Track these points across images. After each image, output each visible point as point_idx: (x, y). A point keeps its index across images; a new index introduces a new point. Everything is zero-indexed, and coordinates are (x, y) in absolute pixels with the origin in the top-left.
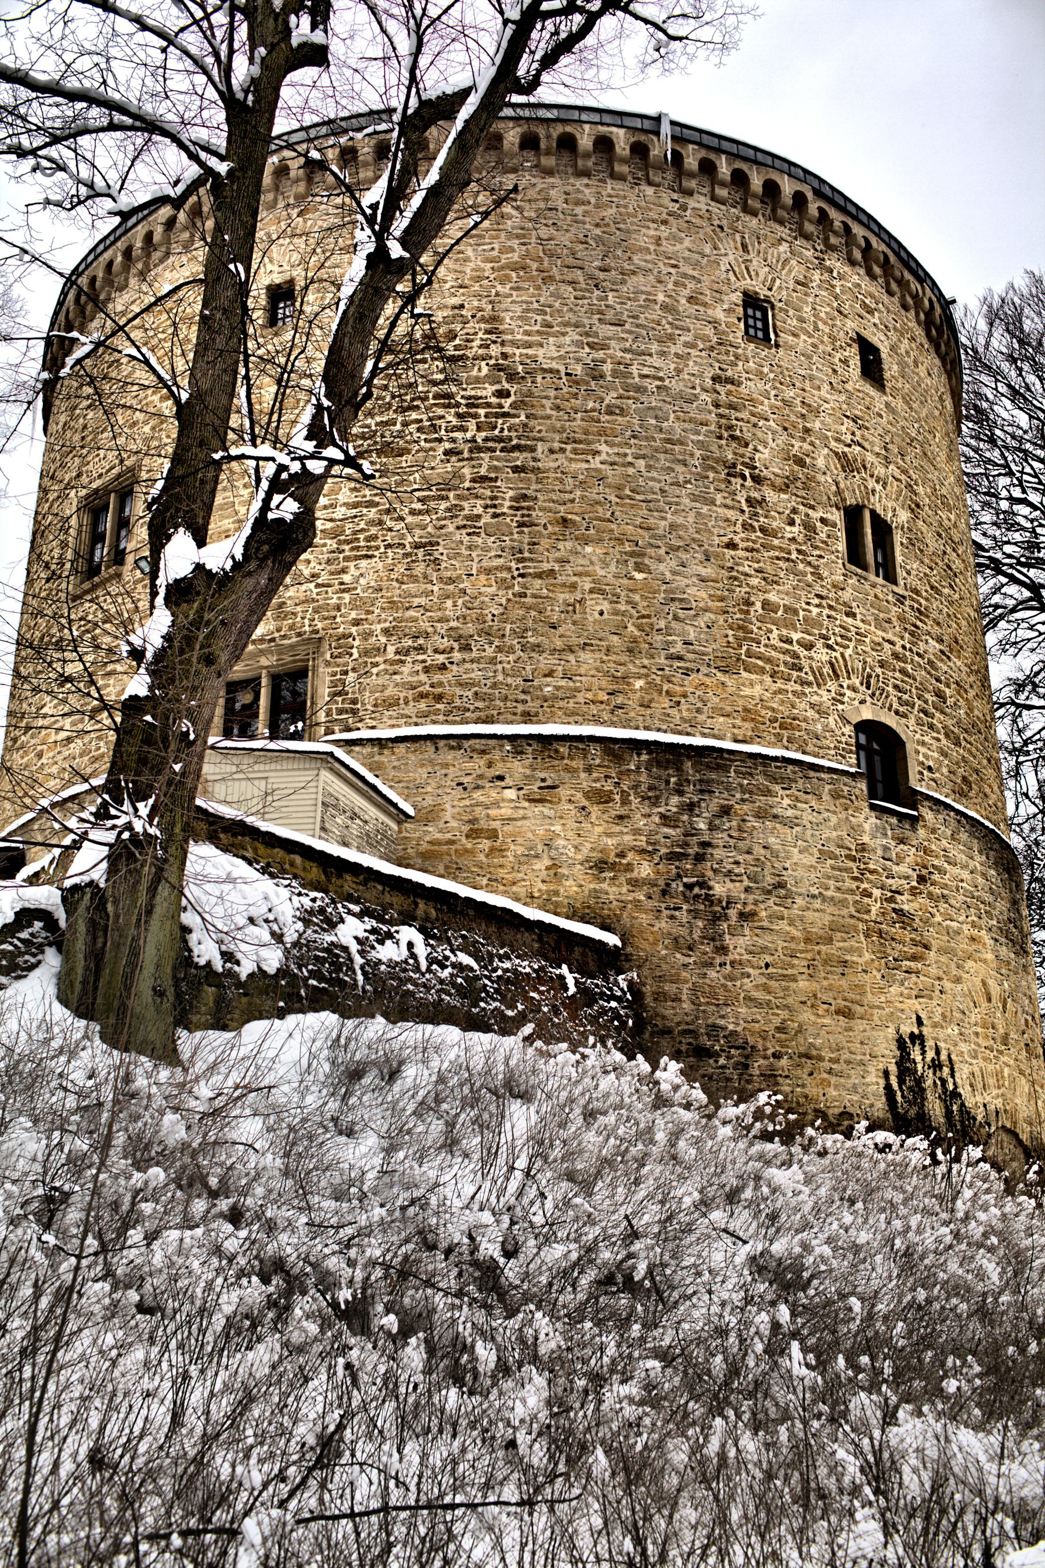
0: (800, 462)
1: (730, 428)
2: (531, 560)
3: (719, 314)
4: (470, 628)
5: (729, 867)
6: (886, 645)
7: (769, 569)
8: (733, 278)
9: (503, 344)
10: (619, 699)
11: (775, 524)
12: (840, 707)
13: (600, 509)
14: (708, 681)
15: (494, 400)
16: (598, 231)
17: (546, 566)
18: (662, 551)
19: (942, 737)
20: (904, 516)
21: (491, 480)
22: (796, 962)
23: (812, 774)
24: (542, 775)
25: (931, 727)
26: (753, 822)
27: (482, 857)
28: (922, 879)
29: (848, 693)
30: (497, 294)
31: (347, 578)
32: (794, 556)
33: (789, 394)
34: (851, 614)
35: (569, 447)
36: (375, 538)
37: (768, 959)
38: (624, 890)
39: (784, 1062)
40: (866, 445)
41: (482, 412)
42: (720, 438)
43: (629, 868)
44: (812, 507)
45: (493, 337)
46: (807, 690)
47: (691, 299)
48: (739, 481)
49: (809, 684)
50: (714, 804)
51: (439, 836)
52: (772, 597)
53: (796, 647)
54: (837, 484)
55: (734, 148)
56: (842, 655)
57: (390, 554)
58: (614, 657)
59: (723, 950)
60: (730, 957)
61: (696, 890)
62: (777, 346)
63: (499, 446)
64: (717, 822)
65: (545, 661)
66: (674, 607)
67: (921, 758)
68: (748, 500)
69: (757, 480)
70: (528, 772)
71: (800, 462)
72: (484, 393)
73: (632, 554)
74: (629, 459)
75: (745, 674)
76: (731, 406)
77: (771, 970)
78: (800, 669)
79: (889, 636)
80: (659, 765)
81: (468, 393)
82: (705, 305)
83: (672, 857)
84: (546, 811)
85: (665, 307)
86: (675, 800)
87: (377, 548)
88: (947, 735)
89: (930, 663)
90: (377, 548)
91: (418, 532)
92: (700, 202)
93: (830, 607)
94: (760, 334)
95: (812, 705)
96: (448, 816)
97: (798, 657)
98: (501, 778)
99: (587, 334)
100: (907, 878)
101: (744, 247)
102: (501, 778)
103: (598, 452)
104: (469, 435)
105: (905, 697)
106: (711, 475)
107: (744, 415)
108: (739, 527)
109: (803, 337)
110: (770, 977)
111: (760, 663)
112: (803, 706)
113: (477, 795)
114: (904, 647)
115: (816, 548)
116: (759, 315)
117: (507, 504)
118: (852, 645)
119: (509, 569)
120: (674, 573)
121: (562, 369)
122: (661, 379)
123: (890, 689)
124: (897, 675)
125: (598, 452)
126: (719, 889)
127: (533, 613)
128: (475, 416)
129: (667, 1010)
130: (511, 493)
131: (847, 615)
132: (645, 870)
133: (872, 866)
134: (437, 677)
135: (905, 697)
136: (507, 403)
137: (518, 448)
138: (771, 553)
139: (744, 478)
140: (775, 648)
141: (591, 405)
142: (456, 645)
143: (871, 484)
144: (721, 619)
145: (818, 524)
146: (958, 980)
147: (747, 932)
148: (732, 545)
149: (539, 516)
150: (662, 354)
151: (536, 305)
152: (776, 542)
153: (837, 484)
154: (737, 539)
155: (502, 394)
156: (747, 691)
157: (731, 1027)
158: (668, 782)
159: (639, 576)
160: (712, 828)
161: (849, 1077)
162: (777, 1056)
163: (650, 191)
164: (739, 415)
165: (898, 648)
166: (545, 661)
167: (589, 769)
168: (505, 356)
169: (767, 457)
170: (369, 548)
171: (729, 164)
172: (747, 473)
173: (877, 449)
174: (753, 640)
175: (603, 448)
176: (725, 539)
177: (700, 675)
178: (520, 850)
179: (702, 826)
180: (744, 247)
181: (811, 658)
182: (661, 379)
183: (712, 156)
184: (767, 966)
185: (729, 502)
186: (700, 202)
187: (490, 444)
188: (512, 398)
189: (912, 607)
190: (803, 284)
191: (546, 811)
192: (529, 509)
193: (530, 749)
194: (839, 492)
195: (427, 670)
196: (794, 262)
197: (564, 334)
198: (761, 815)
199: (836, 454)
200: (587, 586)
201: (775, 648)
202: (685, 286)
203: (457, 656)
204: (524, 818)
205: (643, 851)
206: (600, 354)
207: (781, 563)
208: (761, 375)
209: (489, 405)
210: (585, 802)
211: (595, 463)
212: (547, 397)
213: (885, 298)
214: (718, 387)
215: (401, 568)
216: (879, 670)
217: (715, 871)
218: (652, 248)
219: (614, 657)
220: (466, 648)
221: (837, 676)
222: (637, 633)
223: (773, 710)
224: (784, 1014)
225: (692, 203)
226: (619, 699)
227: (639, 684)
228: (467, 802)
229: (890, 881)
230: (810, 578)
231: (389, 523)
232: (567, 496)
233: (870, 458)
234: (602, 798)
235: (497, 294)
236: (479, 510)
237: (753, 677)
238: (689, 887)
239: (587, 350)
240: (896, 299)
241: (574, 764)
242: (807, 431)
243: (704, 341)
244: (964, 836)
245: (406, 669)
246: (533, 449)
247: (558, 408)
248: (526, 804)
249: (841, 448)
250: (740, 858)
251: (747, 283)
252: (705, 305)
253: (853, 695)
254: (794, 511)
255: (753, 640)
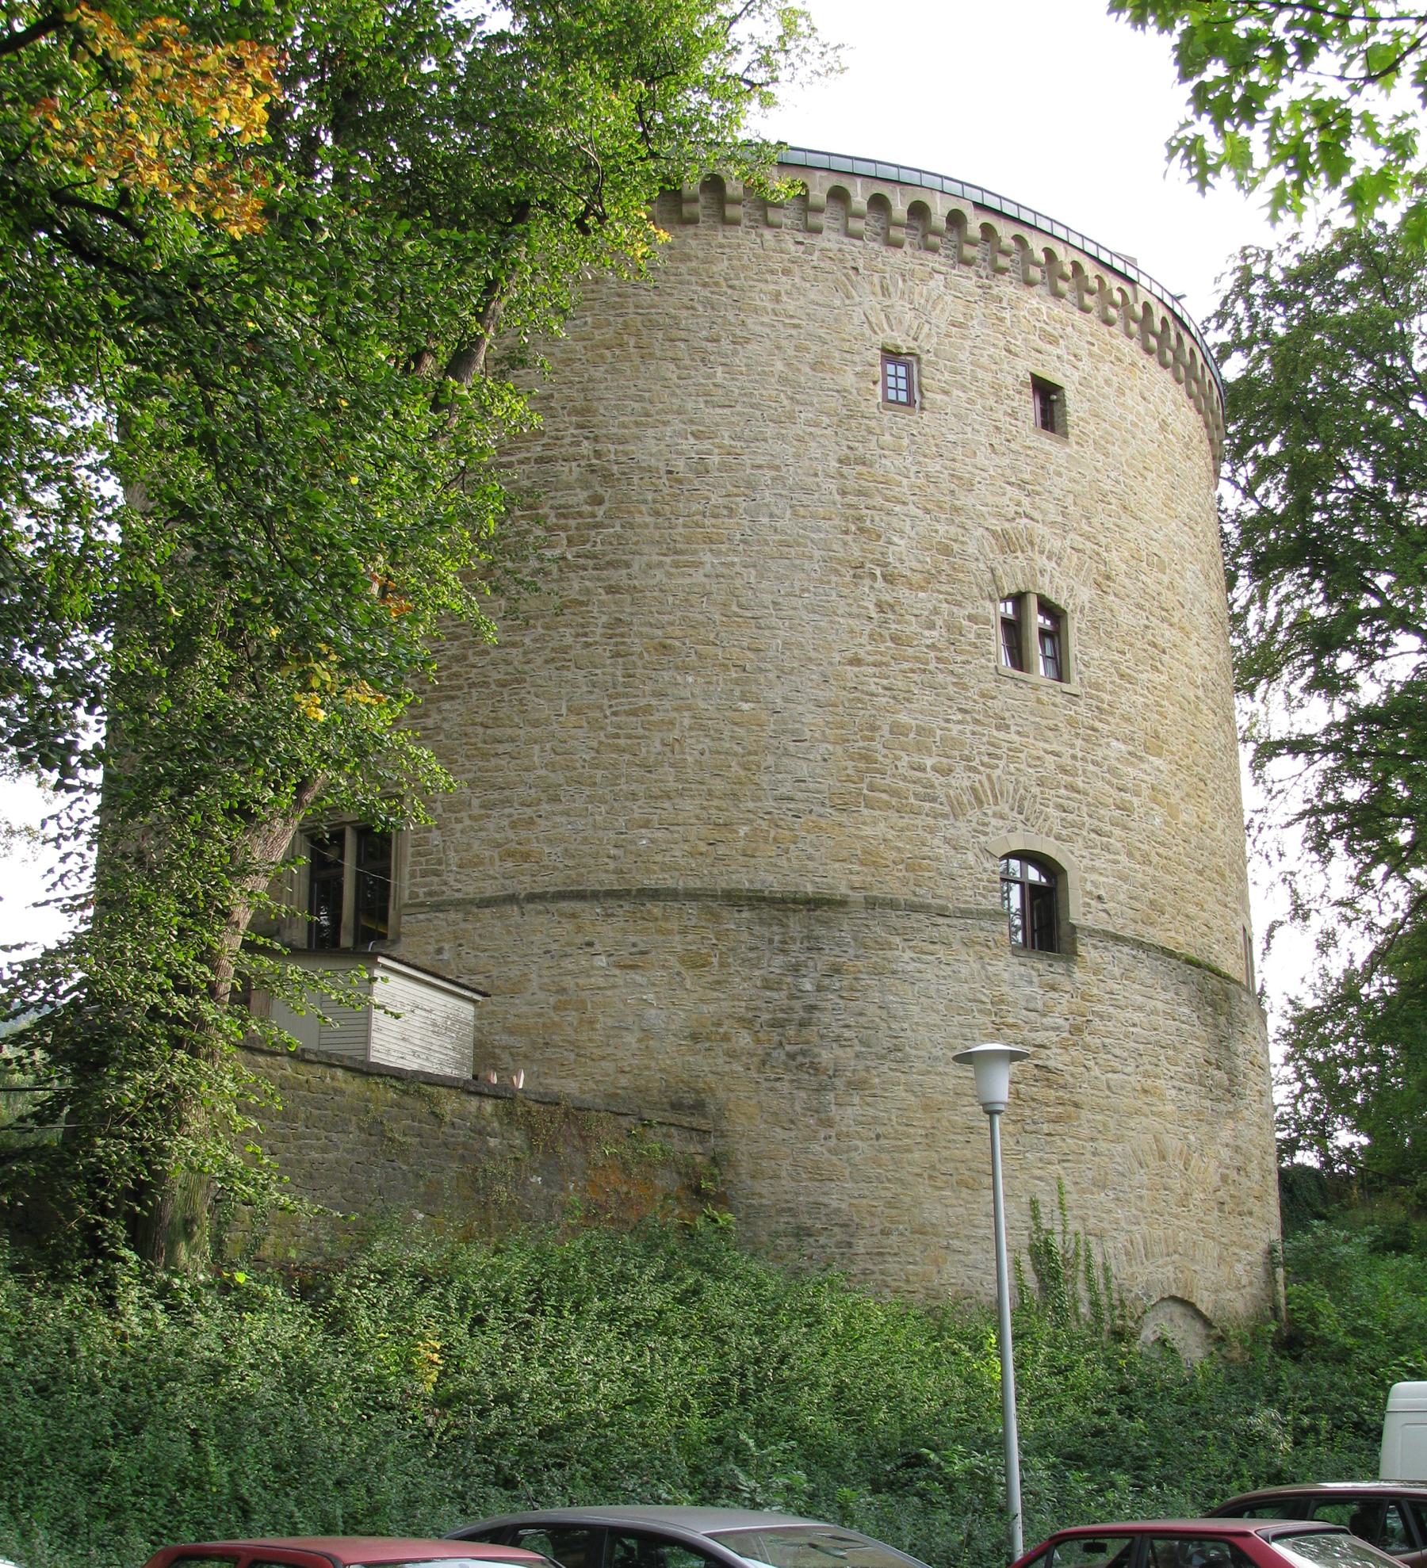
0: (946, 551)
1: (860, 519)
2: (626, 695)
3: (849, 380)
4: (559, 778)
5: (838, 1031)
6: (1050, 758)
7: (900, 684)
8: (868, 332)
9: (596, 439)
10: (721, 850)
11: (909, 630)
12: (983, 839)
13: (702, 631)
14: (823, 822)
15: (587, 508)
16: (706, 293)
17: (642, 702)
18: (772, 676)
19: (1123, 858)
20: (1085, 594)
21: (582, 603)
22: (911, 1130)
23: (940, 920)
24: (633, 939)
25: (1106, 848)
26: (867, 980)
27: (569, 1030)
28: (1076, 1030)
29: (994, 822)
30: (590, 380)
31: (429, 722)
32: (931, 667)
33: (934, 466)
34: (1003, 727)
35: (668, 560)
36: (457, 675)
37: (879, 1130)
38: (720, 1061)
39: (894, 1238)
40: (1036, 515)
41: (572, 523)
42: (846, 533)
43: (726, 1038)
44: (959, 604)
45: (585, 432)
46: (942, 822)
47: (814, 367)
48: (867, 581)
49: (945, 816)
50: (823, 962)
51: (525, 1009)
52: (903, 718)
53: (930, 774)
54: (992, 570)
55: (869, 169)
56: (989, 777)
57: (475, 694)
58: (716, 802)
59: (829, 1123)
60: (837, 1128)
61: (800, 1059)
62: (922, 409)
63: (590, 563)
64: (826, 982)
65: (637, 811)
66: (786, 740)
67: (1089, 887)
68: (879, 605)
69: (889, 579)
70: (619, 936)
71: (946, 551)
72: (572, 500)
73: (737, 682)
74: (738, 568)
75: (865, 812)
76: (860, 493)
77: (883, 1141)
78: (934, 800)
79: (1055, 747)
80: (762, 922)
81: (556, 503)
82: (832, 370)
83: (775, 1024)
84: (638, 978)
85: (783, 380)
86: (779, 960)
87: (460, 688)
88: (1130, 855)
89: (1112, 771)
90: (460, 688)
91: (502, 667)
92: (830, 240)
93: (977, 722)
94: (903, 397)
95: (947, 841)
96: (535, 985)
97: (932, 786)
98: (590, 944)
99: (692, 422)
100: (1056, 1029)
101: (885, 291)
102: (590, 944)
103: (699, 564)
104: (557, 552)
105: (1070, 817)
106: (834, 579)
107: (878, 501)
108: (864, 640)
109: (956, 392)
110: (881, 1150)
111: (884, 796)
112: (936, 842)
113: (567, 964)
114: (1074, 757)
115: (960, 653)
116: (901, 371)
117: (599, 631)
118: (1002, 763)
119: (600, 708)
120: (786, 700)
121: (662, 465)
122: (777, 468)
123: (1050, 810)
124: (1062, 791)
125: (699, 564)
126: (825, 1056)
127: (627, 757)
128: (565, 529)
129: (762, 1187)
130: (604, 619)
131: (998, 728)
132: (744, 1039)
133: (1010, 1020)
134: (524, 834)
135: (1070, 817)
136: (600, 511)
137: (611, 564)
138: (906, 666)
139: (873, 576)
140: (905, 779)
141: (695, 507)
142: (544, 797)
143: (1041, 561)
144: (839, 749)
145: (965, 623)
146: (1118, 1140)
147: (856, 1100)
148: (856, 661)
149: (636, 645)
150: (781, 437)
151: (633, 391)
152: (910, 651)
153: (992, 570)
154: (862, 654)
155: (597, 501)
156: (867, 831)
157: (835, 1204)
158: (771, 941)
159: (745, 706)
160: (820, 988)
161: (969, 1253)
162: (885, 1233)
163: (768, 234)
164: (870, 502)
165: (1066, 760)
166: (637, 811)
167: (684, 932)
168: (598, 454)
169: (902, 551)
170: (453, 688)
171: (864, 188)
172: (878, 573)
173: (1051, 518)
174: (878, 771)
175: (707, 558)
176: (849, 655)
177: (814, 817)
178: (610, 1022)
179: (808, 987)
180: (885, 291)
181: (949, 786)
182: (777, 468)
183: (844, 182)
184: (878, 1137)
185: (855, 610)
186: (830, 240)
187: (581, 561)
188: (607, 505)
189: (1089, 706)
190: (960, 325)
191: (638, 978)
192: (622, 635)
193: (620, 912)
194: (995, 579)
195: (513, 826)
196: (948, 299)
197: (665, 423)
198: (877, 972)
199: (994, 533)
200: (687, 722)
201: (905, 779)
202: (807, 350)
203: (545, 807)
204: (614, 987)
205: (741, 1020)
206: (706, 445)
207: (915, 677)
208: (898, 451)
209: (580, 514)
210: (678, 967)
211: (699, 577)
212: (645, 502)
213: (1078, 315)
214: (845, 470)
215: (485, 711)
216: (1036, 790)
217: (822, 1037)
218: (769, 306)
219: (716, 802)
220: (556, 799)
221: (980, 802)
222: (742, 773)
223: (898, 849)
224: (896, 1188)
225: (820, 241)
226: (721, 850)
227: (743, 830)
228: (555, 972)
229: (1033, 1035)
230: (951, 689)
231: (472, 659)
232: (666, 618)
233: (1040, 529)
234: (695, 962)
235: (590, 380)
236: (569, 640)
237: (877, 813)
238: (792, 1056)
239: (692, 441)
240: (1093, 316)
241: (668, 926)
242: (956, 510)
243: (828, 415)
244: (1143, 973)
245: (491, 825)
246: (628, 565)
247: (657, 514)
248: (617, 972)
249: (997, 525)
250: (851, 1021)
251: (879, 339)
252: (832, 370)
253: (1001, 823)
254: (936, 611)
255: (878, 771)
